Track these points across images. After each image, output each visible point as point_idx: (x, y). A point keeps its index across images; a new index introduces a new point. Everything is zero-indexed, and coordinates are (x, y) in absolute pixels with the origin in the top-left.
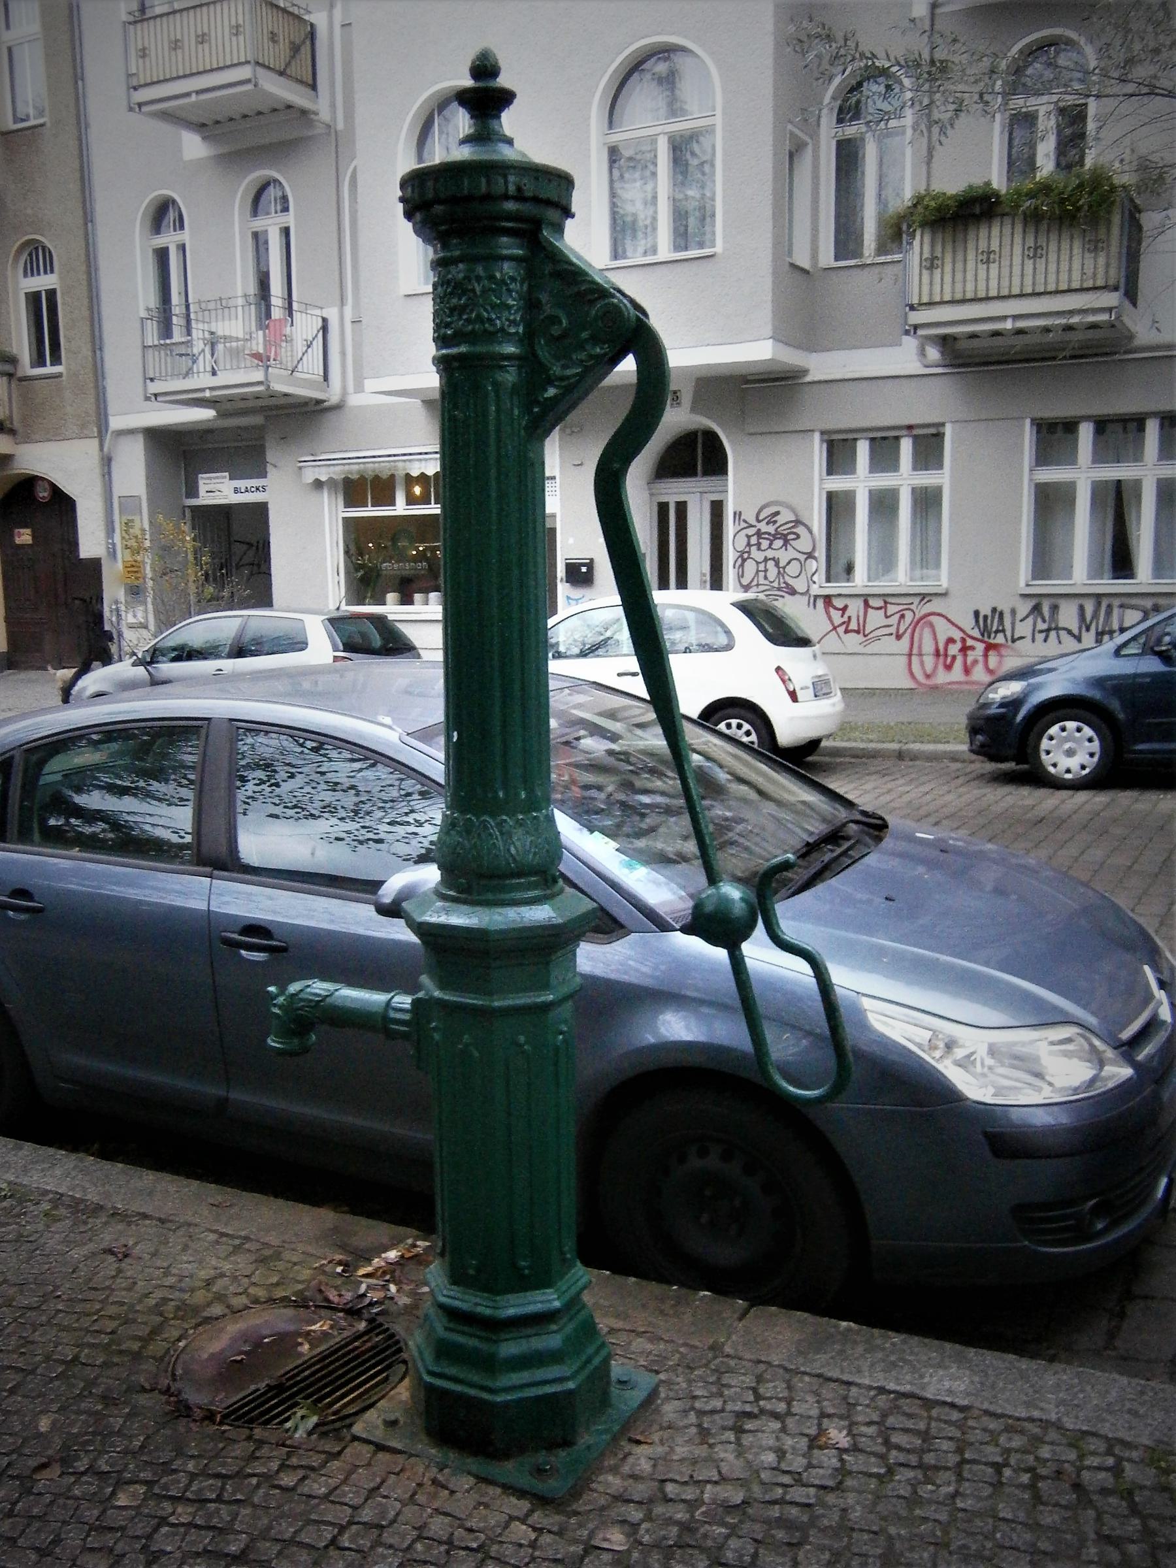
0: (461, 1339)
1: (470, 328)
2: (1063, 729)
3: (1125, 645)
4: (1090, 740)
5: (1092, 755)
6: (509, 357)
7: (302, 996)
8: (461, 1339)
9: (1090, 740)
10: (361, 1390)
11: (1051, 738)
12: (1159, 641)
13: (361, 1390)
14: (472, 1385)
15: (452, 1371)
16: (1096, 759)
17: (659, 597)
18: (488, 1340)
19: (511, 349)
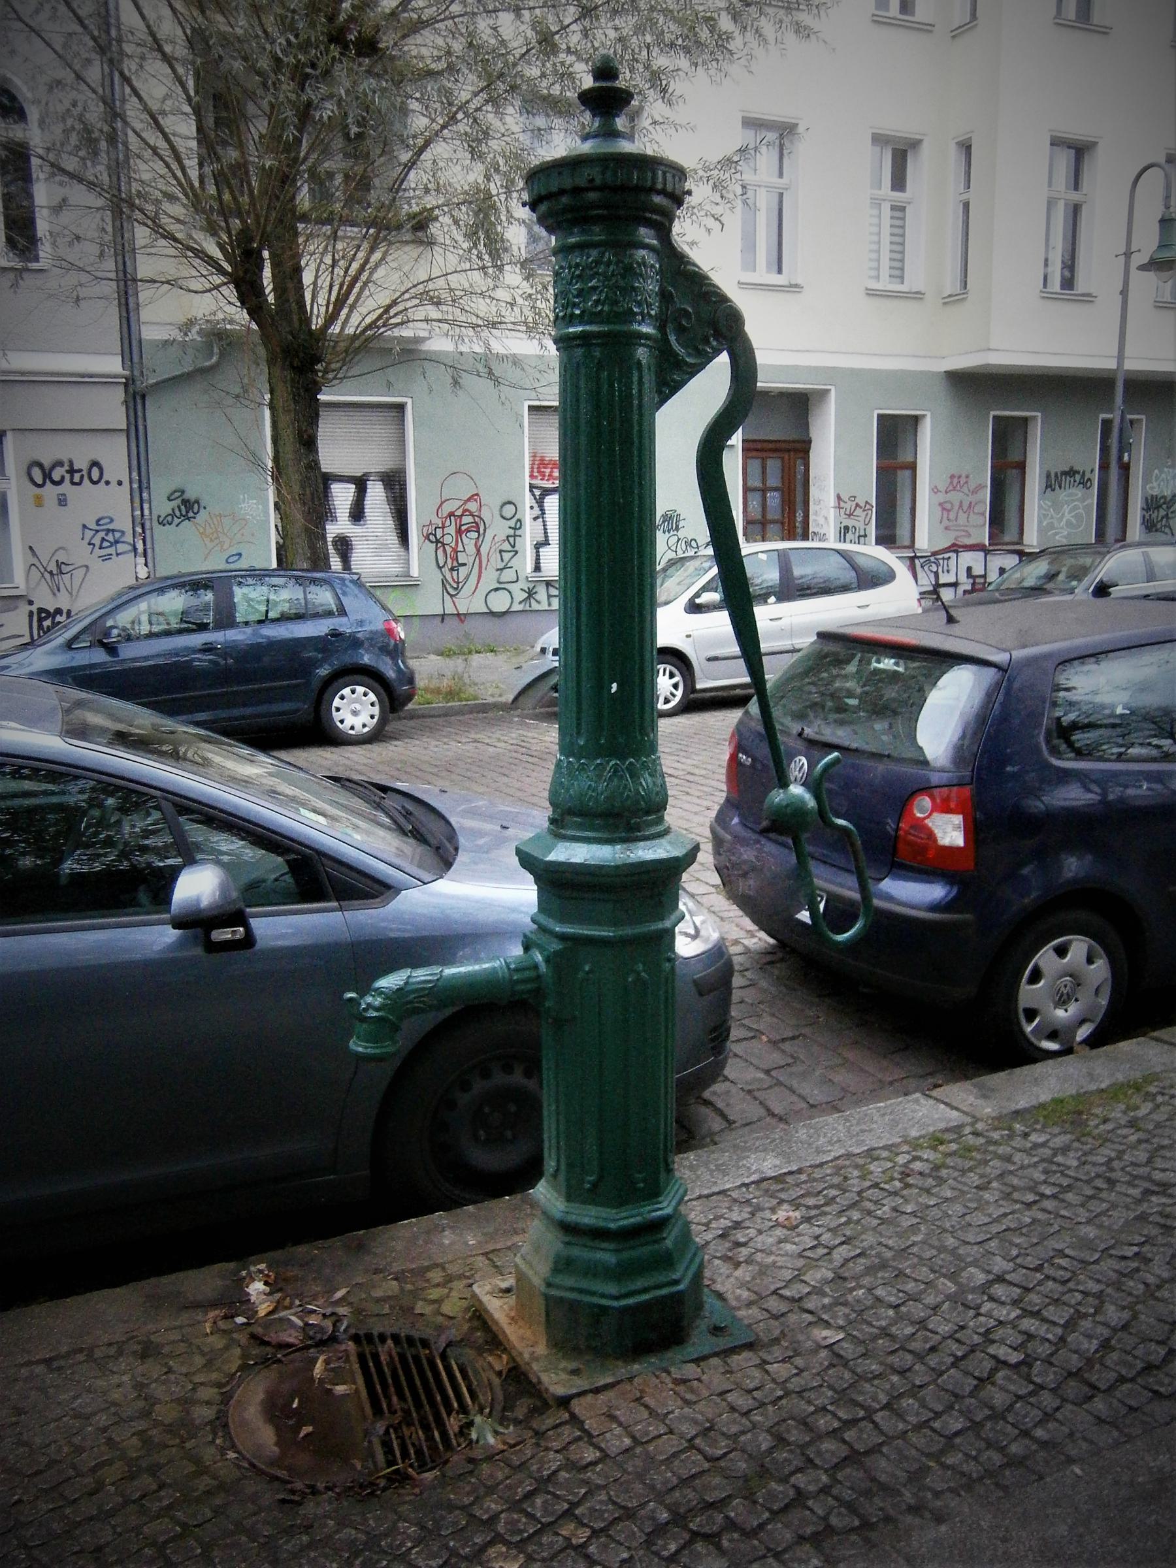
0: (634, 1254)
1: (599, 308)
2: (342, 698)
3: (76, 638)
4: (372, 704)
5: (372, 717)
6: (647, 337)
7: (409, 988)
8: (634, 1254)
9: (372, 704)
10: (421, 1391)
11: (338, 709)
12: (107, 634)
13: (421, 1391)
14: (645, 1290)
15: (639, 1284)
16: (375, 720)
17: (746, 548)
18: (656, 1242)
19: (646, 329)
